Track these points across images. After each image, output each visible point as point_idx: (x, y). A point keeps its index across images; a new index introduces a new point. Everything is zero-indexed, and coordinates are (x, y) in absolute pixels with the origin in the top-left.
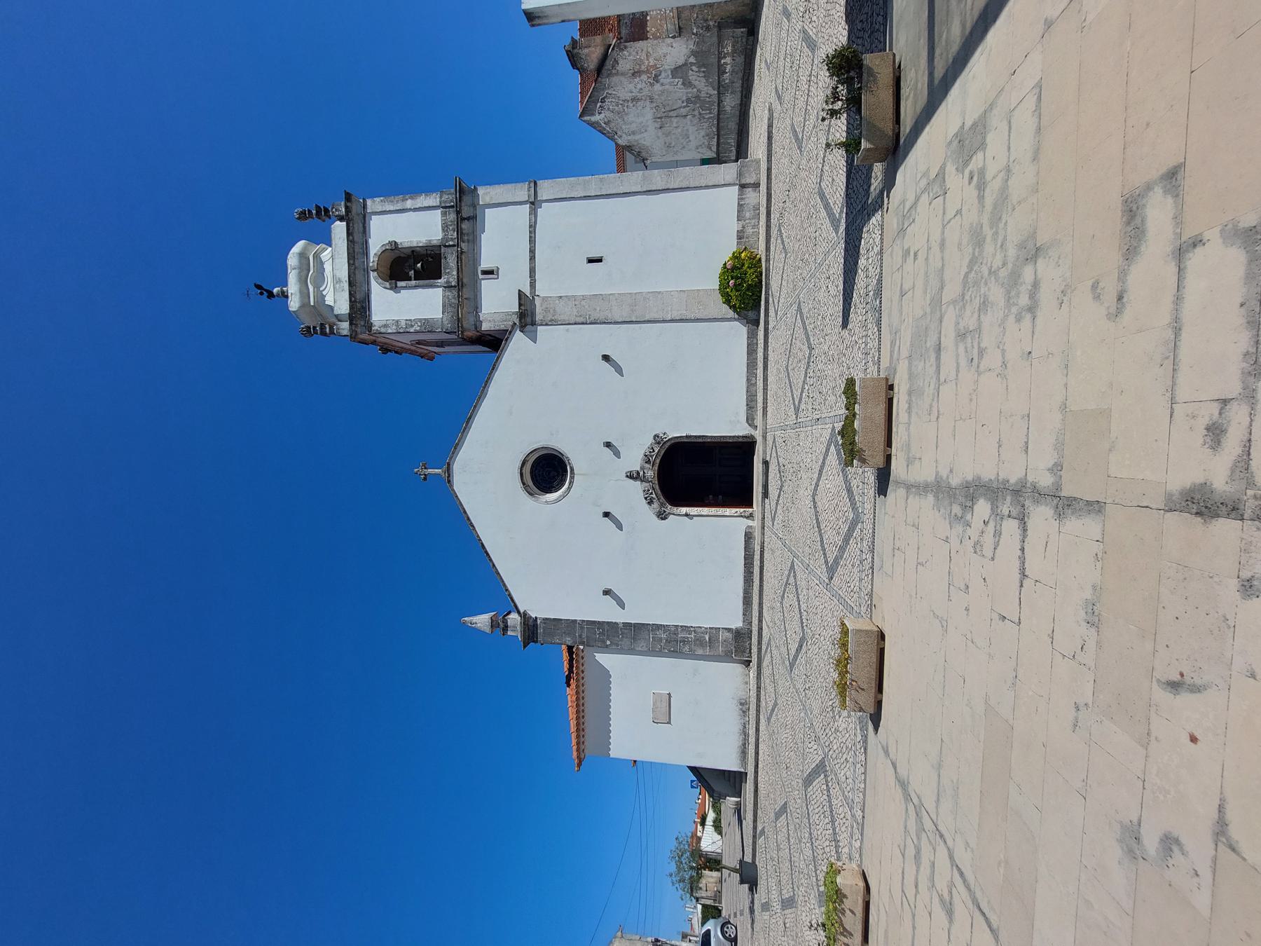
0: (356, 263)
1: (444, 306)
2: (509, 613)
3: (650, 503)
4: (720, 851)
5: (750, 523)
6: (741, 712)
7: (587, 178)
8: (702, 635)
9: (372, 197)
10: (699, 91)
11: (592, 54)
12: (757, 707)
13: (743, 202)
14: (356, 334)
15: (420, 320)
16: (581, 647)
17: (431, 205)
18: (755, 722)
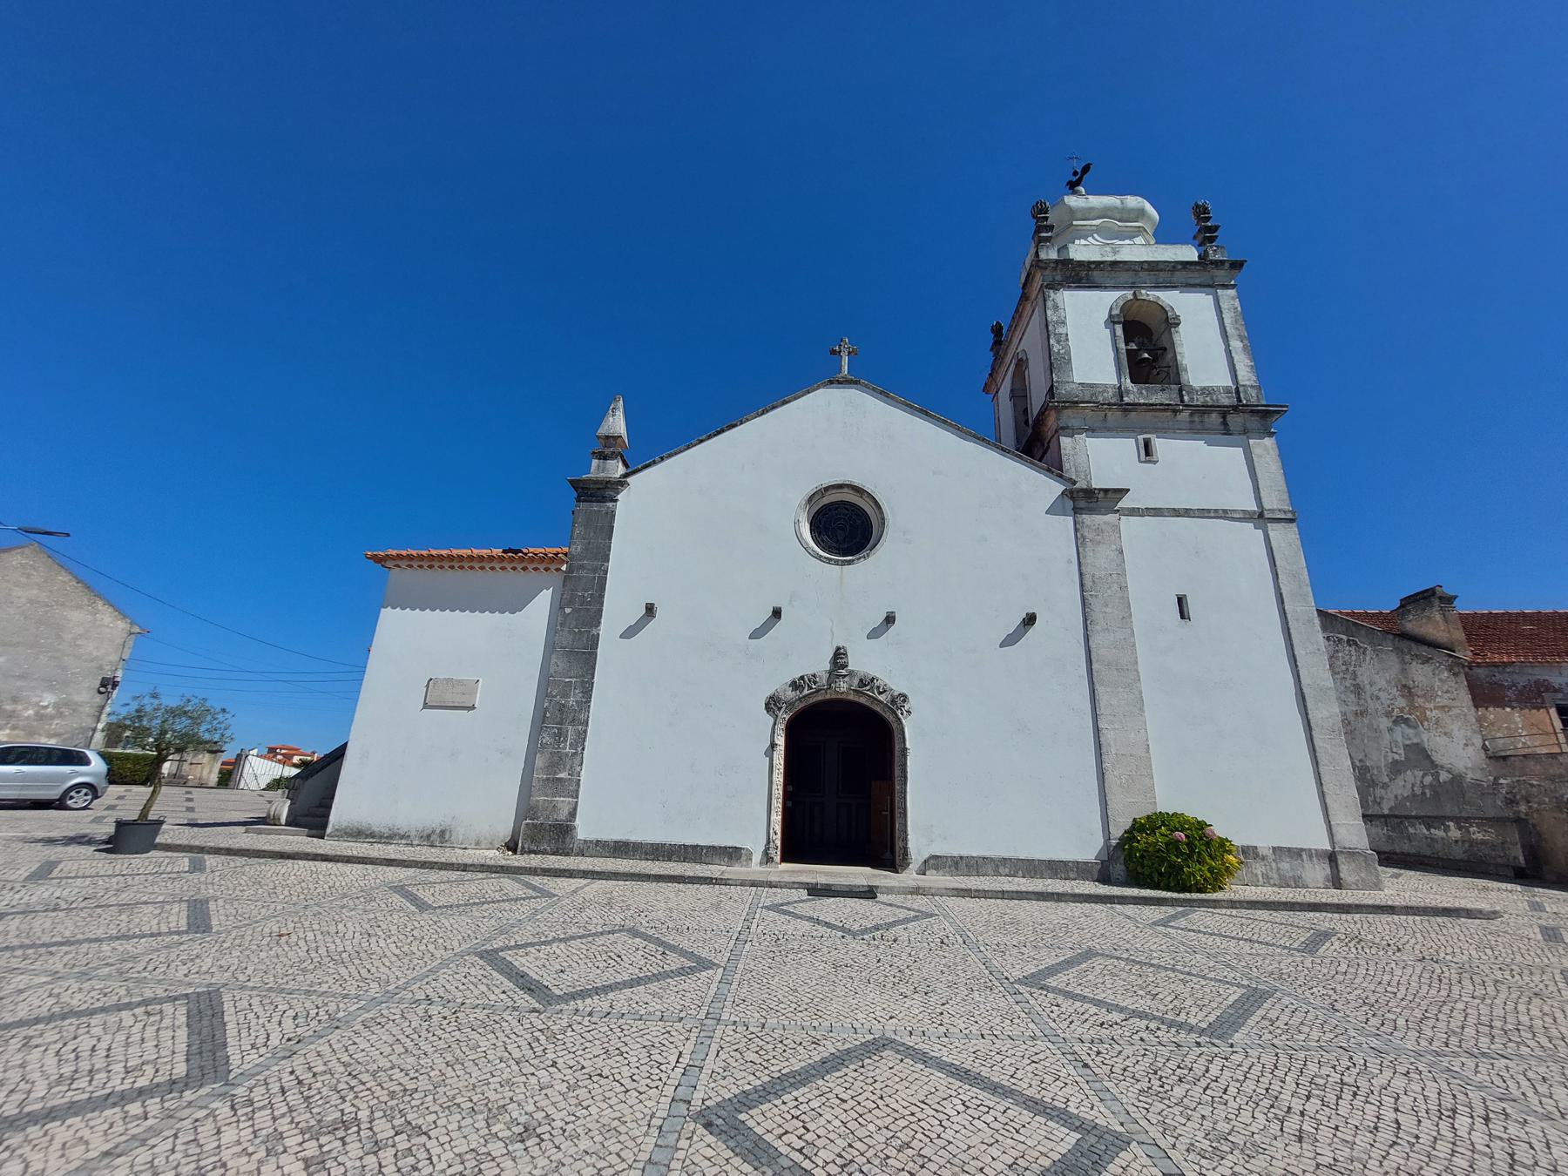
1: (1092, 386)
2: (626, 465)
3: (795, 685)
4: (242, 785)
5: (757, 857)
6: (429, 831)
7: (1311, 599)
8: (568, 767)
9: (1240, 297)
10: (1385, 786)
11: (1433, 625)
12: (431, 863)
13: (1304, 856)
14: (1041, 268)
15: (1068, 353)
16: (564, 568)
17: (1238, 373)
18: (405, 858)
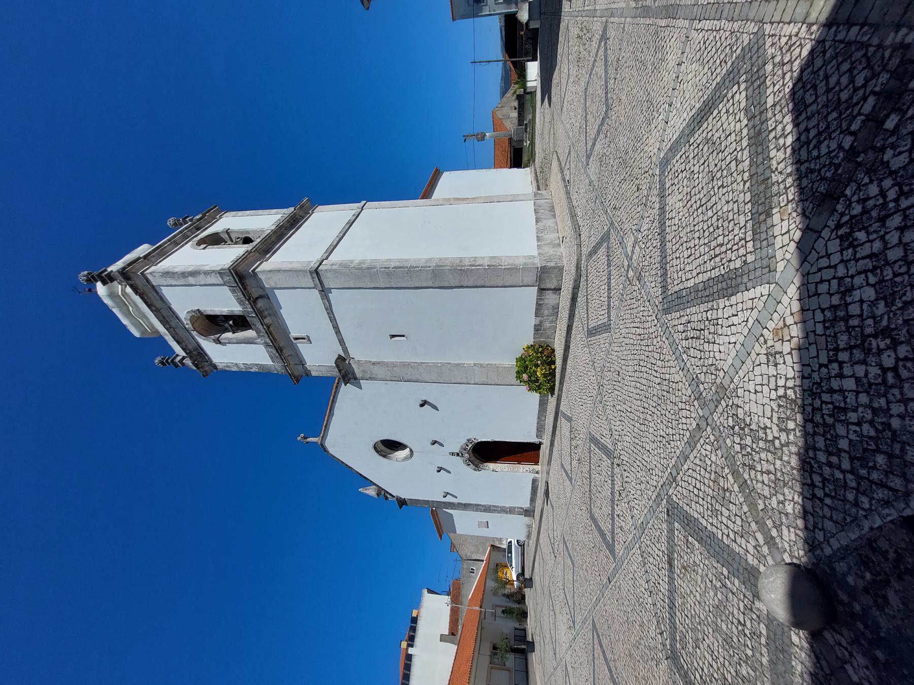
0: (172, 324)
5: (537, 475)
13: (541, 302)
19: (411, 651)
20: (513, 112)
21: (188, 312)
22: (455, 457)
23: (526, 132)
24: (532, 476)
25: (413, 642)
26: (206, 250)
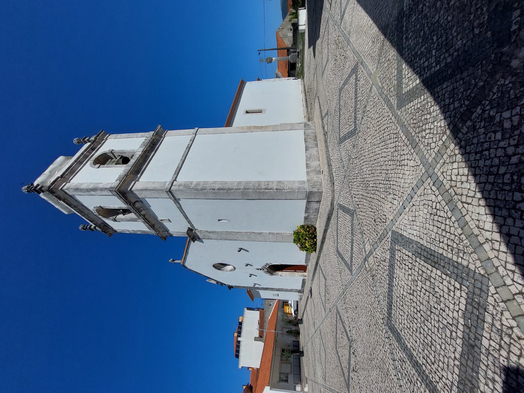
5: (305, 277)
19: (239, 339)
20: (289, 33)
21: (94, 207)
22: (259, 271)
23: (298, 57)
24: (303, 278)
25: (240, 334)
26: (100, 168)
